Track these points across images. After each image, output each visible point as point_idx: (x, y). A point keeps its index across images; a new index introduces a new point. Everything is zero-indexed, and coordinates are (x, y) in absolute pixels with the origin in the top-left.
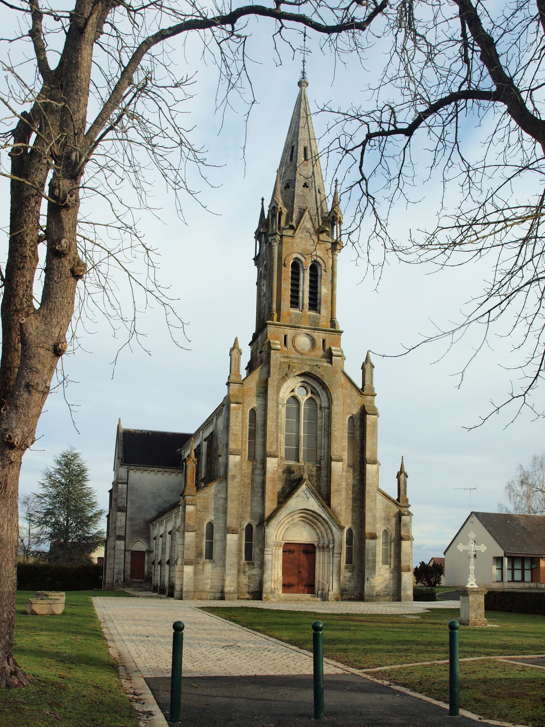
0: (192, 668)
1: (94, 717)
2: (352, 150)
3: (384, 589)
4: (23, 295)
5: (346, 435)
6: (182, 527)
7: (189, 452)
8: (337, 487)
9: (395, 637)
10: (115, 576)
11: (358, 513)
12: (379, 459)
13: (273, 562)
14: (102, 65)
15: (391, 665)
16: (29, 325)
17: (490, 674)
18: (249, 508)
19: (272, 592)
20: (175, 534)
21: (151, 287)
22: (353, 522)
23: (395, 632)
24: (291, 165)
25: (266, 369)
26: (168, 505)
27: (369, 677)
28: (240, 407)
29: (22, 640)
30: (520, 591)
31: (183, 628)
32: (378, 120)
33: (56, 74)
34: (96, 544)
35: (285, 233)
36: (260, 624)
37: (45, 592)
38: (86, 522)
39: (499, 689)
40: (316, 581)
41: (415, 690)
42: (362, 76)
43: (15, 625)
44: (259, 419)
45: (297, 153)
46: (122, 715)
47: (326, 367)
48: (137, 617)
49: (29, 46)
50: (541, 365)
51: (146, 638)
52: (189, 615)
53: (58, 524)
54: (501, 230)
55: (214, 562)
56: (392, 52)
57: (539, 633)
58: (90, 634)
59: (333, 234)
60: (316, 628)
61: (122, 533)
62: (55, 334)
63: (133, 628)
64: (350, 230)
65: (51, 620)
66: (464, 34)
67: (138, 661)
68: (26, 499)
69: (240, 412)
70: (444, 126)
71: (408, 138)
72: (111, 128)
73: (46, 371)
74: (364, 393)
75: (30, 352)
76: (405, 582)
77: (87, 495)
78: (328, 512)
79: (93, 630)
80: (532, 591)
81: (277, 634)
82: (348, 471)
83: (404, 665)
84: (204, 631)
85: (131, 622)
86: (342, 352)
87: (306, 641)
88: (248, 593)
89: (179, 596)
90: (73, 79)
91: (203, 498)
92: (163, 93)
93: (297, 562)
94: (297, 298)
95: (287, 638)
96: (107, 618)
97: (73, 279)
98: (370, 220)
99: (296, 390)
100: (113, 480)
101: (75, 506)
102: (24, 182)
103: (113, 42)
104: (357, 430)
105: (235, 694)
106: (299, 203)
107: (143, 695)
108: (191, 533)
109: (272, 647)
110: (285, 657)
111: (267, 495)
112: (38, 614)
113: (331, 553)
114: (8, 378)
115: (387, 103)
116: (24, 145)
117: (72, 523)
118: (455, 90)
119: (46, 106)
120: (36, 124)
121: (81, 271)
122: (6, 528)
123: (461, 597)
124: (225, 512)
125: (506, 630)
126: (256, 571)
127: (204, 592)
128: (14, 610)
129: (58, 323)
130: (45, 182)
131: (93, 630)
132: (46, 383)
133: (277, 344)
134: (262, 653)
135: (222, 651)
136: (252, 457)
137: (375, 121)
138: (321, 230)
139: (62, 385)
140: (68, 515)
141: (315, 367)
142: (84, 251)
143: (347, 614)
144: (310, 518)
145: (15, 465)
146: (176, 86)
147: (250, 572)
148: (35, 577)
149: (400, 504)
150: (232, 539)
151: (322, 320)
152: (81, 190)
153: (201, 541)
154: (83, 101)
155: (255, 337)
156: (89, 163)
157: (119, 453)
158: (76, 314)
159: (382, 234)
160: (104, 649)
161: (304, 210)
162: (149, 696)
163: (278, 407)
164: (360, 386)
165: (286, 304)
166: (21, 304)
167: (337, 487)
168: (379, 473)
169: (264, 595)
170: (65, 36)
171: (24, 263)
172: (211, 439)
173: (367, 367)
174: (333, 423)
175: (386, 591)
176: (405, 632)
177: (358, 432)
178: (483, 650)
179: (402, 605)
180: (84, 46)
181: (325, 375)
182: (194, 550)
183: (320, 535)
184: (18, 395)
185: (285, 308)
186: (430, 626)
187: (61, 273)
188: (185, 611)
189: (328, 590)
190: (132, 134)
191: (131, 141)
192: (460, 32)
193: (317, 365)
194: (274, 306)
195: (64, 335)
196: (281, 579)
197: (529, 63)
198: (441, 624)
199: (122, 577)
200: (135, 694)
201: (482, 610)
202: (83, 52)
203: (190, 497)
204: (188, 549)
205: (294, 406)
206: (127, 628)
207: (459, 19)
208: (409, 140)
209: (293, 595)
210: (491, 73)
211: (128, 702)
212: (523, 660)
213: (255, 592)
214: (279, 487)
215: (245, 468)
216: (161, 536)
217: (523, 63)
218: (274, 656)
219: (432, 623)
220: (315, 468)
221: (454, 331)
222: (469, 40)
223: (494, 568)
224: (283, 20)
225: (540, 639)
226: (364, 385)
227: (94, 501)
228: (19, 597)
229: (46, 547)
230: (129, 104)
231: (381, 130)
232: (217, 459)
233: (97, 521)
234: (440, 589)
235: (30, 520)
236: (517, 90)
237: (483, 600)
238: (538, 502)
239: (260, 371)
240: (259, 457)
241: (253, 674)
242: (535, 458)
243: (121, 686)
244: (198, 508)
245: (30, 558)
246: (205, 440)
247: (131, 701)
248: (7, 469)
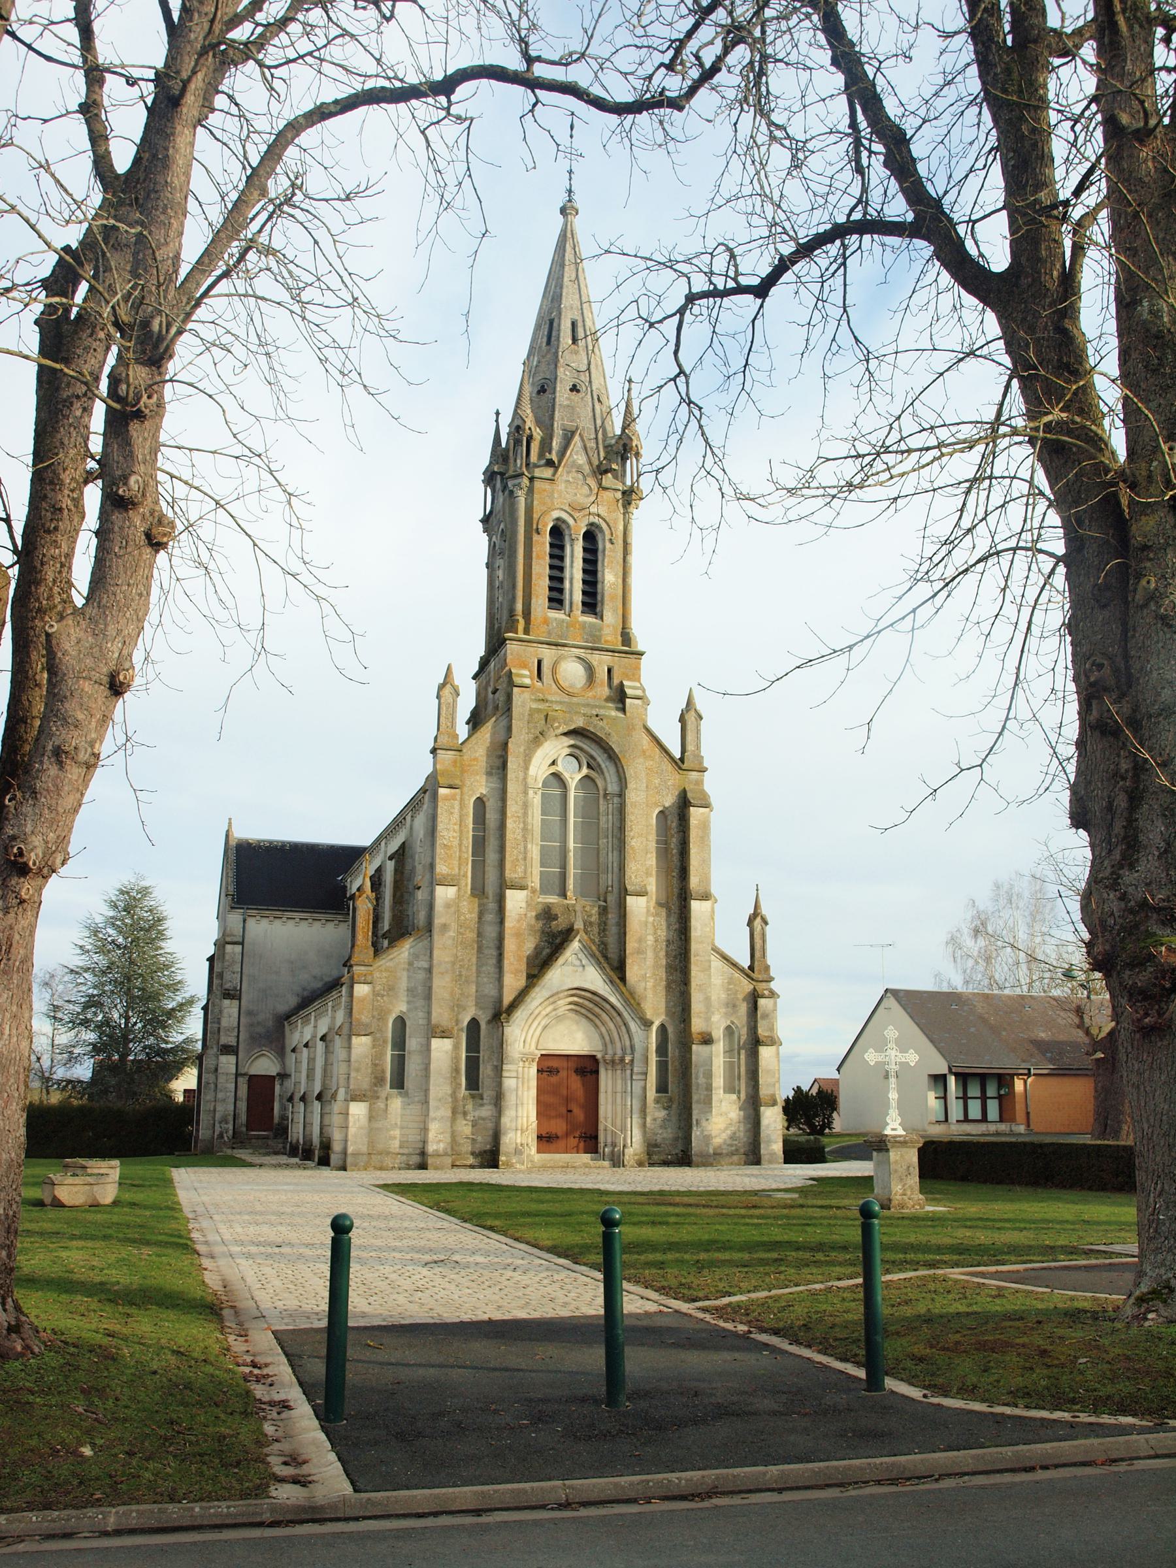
0: (367, 1309)
1: (174, 1416)
2: (660, 322)
3: (729, 1142)
4: (54, 581)
5: (653, 845)
6: (346, 1026)
7: (359, 881)
8: (636, 945)
9: (755, 1235)
10: (217, 1125)
11: (678, 994)
12: (714, 890)
13: (520, 1093)
14: (211, 166)
15: (749, 1292)
16: (64, 636)
17: (938, 1305)
18: (473, 988)
19: (518, 1152)
20: (332, 1041)
21: (296, 566)
22: (669, 1013)
23: (753, 1225)
24: (548, 351)
25: (503, 723)
26: (320, 985)
27: (708, 1317)
29: (33, 1259)
30: (982, 1139)
31: (348, 1230)
32: (707, 270)
33: (127, 179)
34: (182, 1063)
35: (537, 473)
36: (497, 1216)
37: (81, 1161)
38: (161, 1020)
39: (958, 1335)
40: (601, 1127)
41: (797, 1342)
42: (677, 194)
43: (20, 1229)
44: (491, 817)
45: (559, 330)
46: (229, 1411)
47: (615, 718)
48: (259, 1208)
49: (78, 129)
50: (1009, 709)
51: (277, 1250)
52: (359, 1201)
53: (108, 1025)
54: (932, 462)
55: (406, 1095)
56: (729, 153)
57: (1023, 1221)
58: (166, 1244)
59: (624, 475)
60: (608, 1222)
61: (232, 1041)
62: (113, 652)
63: (252, 1229)
64: (659, 464)
65: (91, 1217)
66: (853, 124)
67: (260, 1296)
68: (47, 976)
69: (457, 804)
70: (823, 282)
71: (759, 301)
72: (226, 274)
73: (94, 724)
74: (684, 767)
75: (64, 688)
76: (768, 1126)
77: (167, 967)
78: (621, 994)
79: (172, 1236)
80: (1003, 1139)
81: (530, 1234)
82: (657, 915)
83: (774, 1292)
84: (388, 1233)
85: (246, 1217)
86: (644, 691)
87: (586, 1248)
88: (473, 1153)
89: (340, 1163)
90: (158, 188)
91: (386, 970)
92: (322, 209)
93: (565, 1092)
94: (561, 591)
95: (549, 1243)
96: (200, 1209)
97: (149, 550)
98: (694, 446)
99: (559, 762)
100: (216, 937)
101: (143, 989)
102: (62, 370)
103: (232, 125)
104: (673, 836)
105: (451, 1360)
106: (563, 419)
107: (271, 1368)
108: (363, 1038)
109: (521, 1262)
110: (545, 1281)
111: (506, 962)
112: (64, 1206)
113: (628, 1072)
114: (21, 738)
115: (721, 240)
116: (64, 300)
117: (136, 1023)
118: (841, 219)
119: (108, 231)
120: (87, 267)
121: (165, 535)
122: (7, 1032)
123: (875, 1154)
124: (428, 997)
125: (960, 1216)
126: (486, 1111)
127: (388, 1153)
128: (18, 1199)
129: (119, 632)
130: (101, 372)
131: (172, 1236)
132: (92, 747)
133: (524, 676)
134: (502, 1275)
135: (425, 1271)
136: (478, 890)
137: (701, 271)
138: (603, 468)
139: (122, 752)
140: (129, 1007)
141: (594, 718)
142: (170, 500)
143: (661, 1193)
144: (588, 1005)
145: (29, 907)
146: (348, 198)
148: (60, 1131)
149: (754, 976)
150: (441, 1048)
151: (606, 631)
152: (168, 386)
153: (380, 1055)
154: (175, 225)
155: (484, 663)
156: (185, 337)
157: (227, 884)
158: (153, 617)
159: (717, 472)
160: (194, 1274)
161: (573, 433)
162: (282, 1369)
163: (526, 793)
164: (677, 754)
165: (540, 602)
166: (50, 597)
167: (636, 945)
168: (716, 918)
169: (502, 1158)
170: (145, 113)
171: (57, 520)
172: (401, 855)
173: (688, 717)
174: (628, 824)
175: (731, 1145)
176: (772, 1225)
177: (674, 840)
178: (920, 1257)
179: (763, 1172)
180: (179, 128)
181: (613, 734)
182: (369, 1071)
183: (607, 1038)
184: (38, 770)
185: (539, 610)
186: (818, 1213)
187: (126, 538)
188: (352, 1192)
189: (624, 1146)
190: (265, 285)
191: (262, 298)
192: (847, 121)
194: (519, 607)
195: (130, 655)
196: (535, 1125)
197: (967, 176)
198: (838, 1208)
199: (231, 1127)
200: (254, 1365)
201: (914, 1180)
202: (178, 140)
203: (363, 968)
204: (358, 1070)
205: (557, 792)
206: (239, 1230)
207: (844, 97)
208: (762, 306)
209: (557, 1156)
210: (903, 190)
211: (242, 1382)
212: (993, 1276)
213: (485, 1152)
214: (529, 946)
215: (465, 910)
216: (306, 1045)
217: (957, 176)
218: (525, 1280)
219: (821, 1207)
220: (596, 909)
221: (851, 647)
222: (863, 134)
223: (931, 1095)
224: (537, 91)
225: (1025, 1232)
226: (683, 750)
227: (179, 978)
228: (29, 1171)
229: (84, 1071)
230: (260, 231)
231: (712, 287)
232: (412, 894)
233: (183, 1017)
234: (832, 1140)
235: (55, 1018)
236: (950, 220)
237: (915, 1159)
238: (1006, 968)
239: (494, 727)
240: (491, 890)
241: (485, 1317)
242: (998, 886)
243: (228, 1350)
244: (378, 988)
245: (52, 1094)
246: (391, 858)
247: (246, 1380)
248: (12, 915)
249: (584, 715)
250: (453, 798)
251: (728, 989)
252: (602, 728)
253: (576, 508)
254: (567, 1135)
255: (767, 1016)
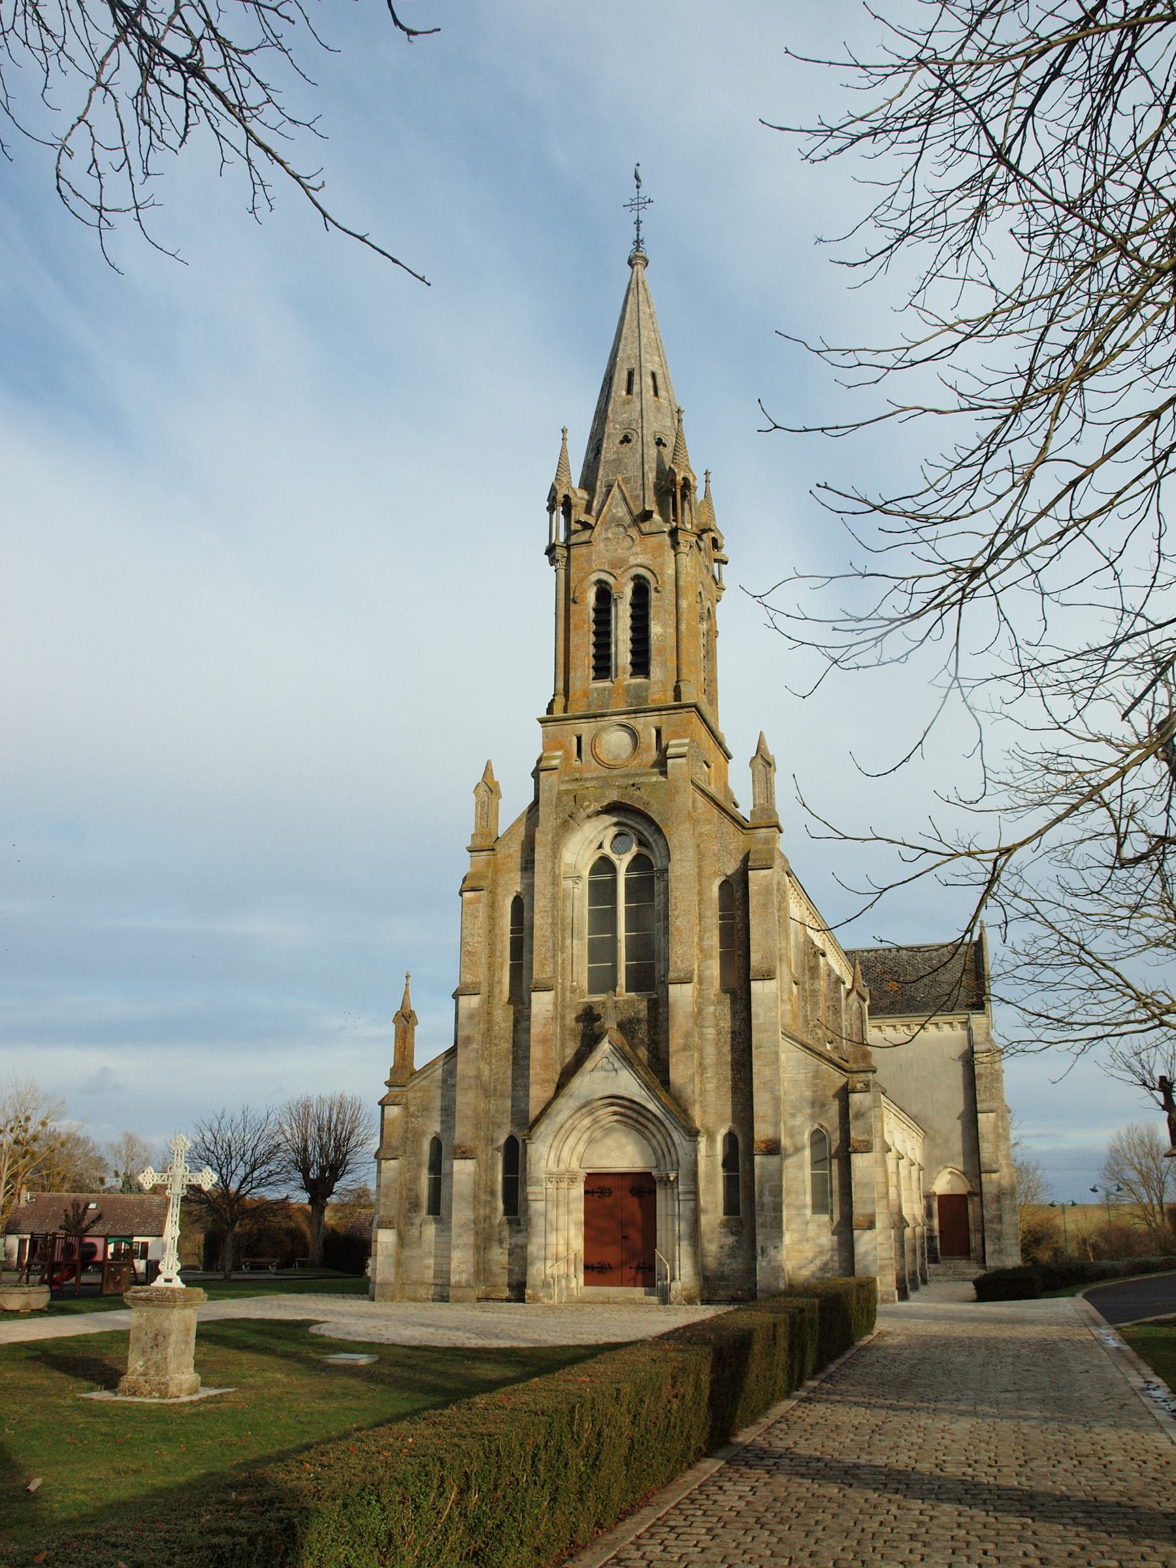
3: (819, 1275)
5: (537, 933)
18: (509, 1103)
28: (480, 897)
47: (654, 784)
82: (719, 1003)
91: (420, 1090)
127: (423, 1283)
144: (632, 1115)
147: (513, 1241)
153: (416, 1179)
169: (529, 1291)
173: (763, 761)
181: (653, 802)
185: (578, 684)
193: (633, 785)
204: (386, 1196)
220: (645, 1003)
244: (412, 1109)
249: (618, 787)
250: (478, 901)
251: (816, 1085)
252: (639, 798)
253: (618, 563)
254: (622, 1265)
255: (863, 1115)
